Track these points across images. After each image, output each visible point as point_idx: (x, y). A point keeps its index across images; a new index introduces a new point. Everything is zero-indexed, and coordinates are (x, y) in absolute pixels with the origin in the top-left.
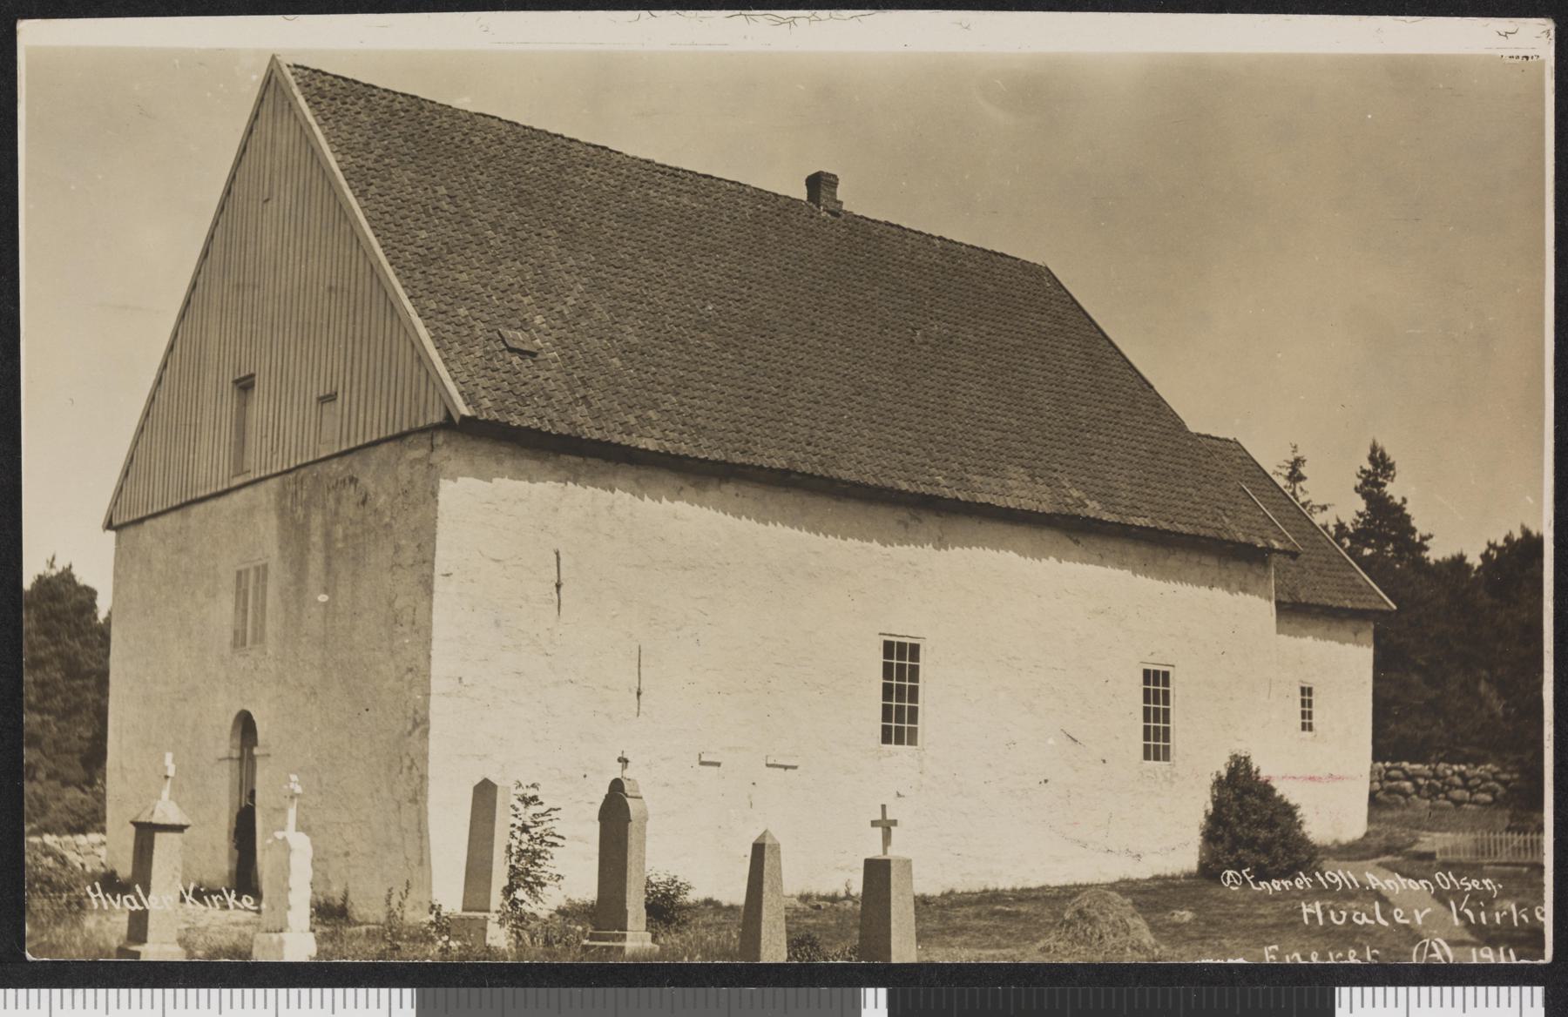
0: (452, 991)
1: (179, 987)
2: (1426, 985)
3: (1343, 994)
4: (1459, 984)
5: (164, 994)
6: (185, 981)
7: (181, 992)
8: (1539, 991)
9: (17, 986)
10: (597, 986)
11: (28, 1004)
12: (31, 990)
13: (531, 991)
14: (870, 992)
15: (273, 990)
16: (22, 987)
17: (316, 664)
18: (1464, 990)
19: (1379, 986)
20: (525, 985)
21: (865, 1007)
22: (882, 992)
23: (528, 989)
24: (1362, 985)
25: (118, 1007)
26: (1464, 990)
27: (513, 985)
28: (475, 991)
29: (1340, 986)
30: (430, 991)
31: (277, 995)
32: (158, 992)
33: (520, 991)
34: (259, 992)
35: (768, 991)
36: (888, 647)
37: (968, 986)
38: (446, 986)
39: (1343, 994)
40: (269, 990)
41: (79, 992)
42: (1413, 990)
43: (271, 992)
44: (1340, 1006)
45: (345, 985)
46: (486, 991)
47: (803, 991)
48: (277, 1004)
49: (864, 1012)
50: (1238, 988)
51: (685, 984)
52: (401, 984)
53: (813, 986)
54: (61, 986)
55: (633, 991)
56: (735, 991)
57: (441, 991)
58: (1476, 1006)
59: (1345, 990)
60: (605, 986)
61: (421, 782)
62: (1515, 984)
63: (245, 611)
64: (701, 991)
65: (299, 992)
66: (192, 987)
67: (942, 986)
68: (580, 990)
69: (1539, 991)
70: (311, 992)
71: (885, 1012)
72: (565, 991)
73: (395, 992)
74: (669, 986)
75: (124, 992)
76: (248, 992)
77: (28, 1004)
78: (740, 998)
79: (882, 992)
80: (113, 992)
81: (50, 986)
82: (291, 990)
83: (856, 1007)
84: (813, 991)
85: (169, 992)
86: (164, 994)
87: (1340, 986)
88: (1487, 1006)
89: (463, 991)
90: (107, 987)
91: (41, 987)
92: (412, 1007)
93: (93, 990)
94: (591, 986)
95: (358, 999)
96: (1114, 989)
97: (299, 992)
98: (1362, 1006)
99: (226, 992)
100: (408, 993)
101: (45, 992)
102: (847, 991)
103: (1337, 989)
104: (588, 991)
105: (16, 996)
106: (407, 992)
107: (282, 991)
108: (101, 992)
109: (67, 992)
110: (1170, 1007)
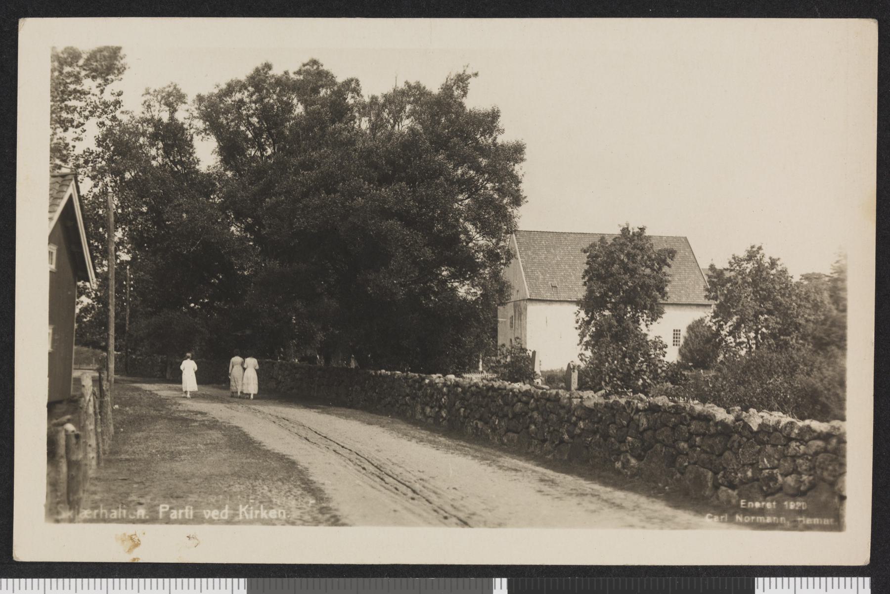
0: (267, 580)
1: (116, 577)
2: (805, 576)
3: (759, 581)
4: (823, 576)
5: (139, 581)
6: (119, 574)
7: (117, 580)
8: (868, 580)
9: (26, 577)
10: (347, 577)
11: (13, 591)
12: (47, 579)
13: (310, 580)
14: (498, 580)
15: (74, 579)
16: (29, 578)
17: (815, 332)
18: (188, 580)
19: (779, 577)
20: (308, 576)
21: (495, 589)
22: (505, 580)
23: (309, 579)
24: (770, 576)
25: (63, 589)
26: (188, 580)
27: (300, 576)
28: (279, 580)
29: (758, 577)
30: (254, 580)
31: (151, 582)
32: (104, 580)
33: (304, 580)
34: (160, 580)
35: (442, 579)
36: (674, 331)
37: (659, 577)
38: (263, 577)
39: (759, 581)
40: (165, 579)
41: (60, 580)
42: (798, 579)
43: (167, 580)
44: (758, 588)
45: (208, 576)
46: (286, 580)
47: (460, 580)
48: (170, 587)
49: (494, 591)
50: (701, 579)
51: (395, 576)
52: (238, 576)
53: (466, 577)
54: (51, 577)
55: (367, 580)
56: (423, 579)
57: (261, 580)
58: (114, 589)
59: (760, 579)
60: (351, 577)
61: (220, 429)
62: (854, 576)
63: (52, 259)
64: (404, 580)
65: (182, 580)
66: (811, 576)
67: (538, 576)
68: (337, 579)
69: (868, 580)
70: (38, 581)
71: (869, 590)
72: (329, 580)
73: (235, 580)
74: (386, 577)
75: (85, 580)
76: (154, 580)
77: (13, 591)
78: (426, 584)
79: (505, 580)
80: (79, 580)
81: (45, 577)
82: (178, 579)
83: (490, 589)
84: (466, 580)
85: (110, 580)
86: (139, 581)
87: (758, 577)
88: (782, 588)
89: (273, 580)
90: (76, 577)
91: (765, 577)
92: (245, 589)
93: (5, 579)
94: (344, 577)
95: (212, 584)
96: (633, 579)
97: (182, 580)
98: (145, 589)
99: (142, 580)
100: (242, 581)
101: (41, 580)
102: (485, 580)
103: (756, 579)
104: (342, 580)
105: (26, 583)
106: (242, 580)
107: (173, 580)
108: (73, 580)
109: (54, 580)
110: (739, 589)
